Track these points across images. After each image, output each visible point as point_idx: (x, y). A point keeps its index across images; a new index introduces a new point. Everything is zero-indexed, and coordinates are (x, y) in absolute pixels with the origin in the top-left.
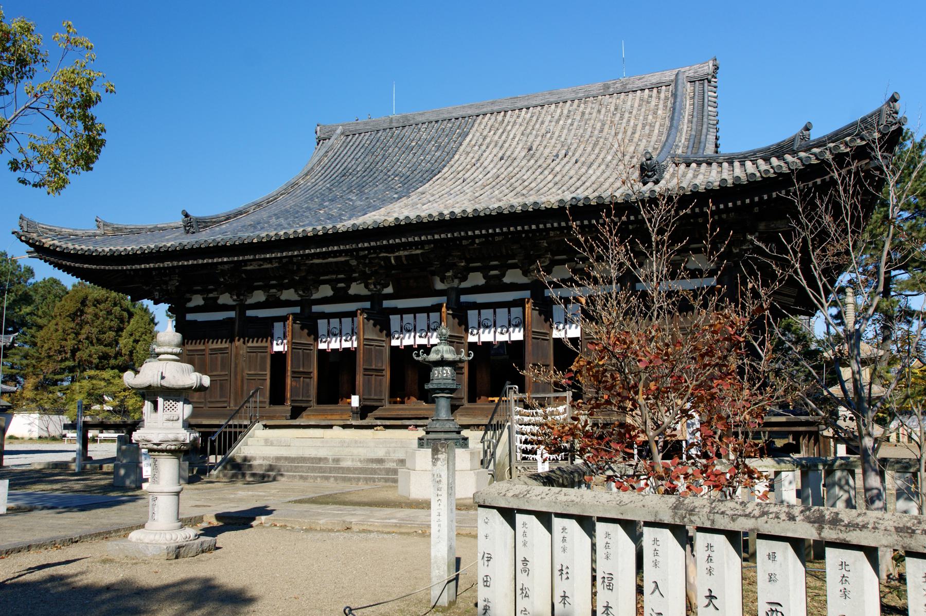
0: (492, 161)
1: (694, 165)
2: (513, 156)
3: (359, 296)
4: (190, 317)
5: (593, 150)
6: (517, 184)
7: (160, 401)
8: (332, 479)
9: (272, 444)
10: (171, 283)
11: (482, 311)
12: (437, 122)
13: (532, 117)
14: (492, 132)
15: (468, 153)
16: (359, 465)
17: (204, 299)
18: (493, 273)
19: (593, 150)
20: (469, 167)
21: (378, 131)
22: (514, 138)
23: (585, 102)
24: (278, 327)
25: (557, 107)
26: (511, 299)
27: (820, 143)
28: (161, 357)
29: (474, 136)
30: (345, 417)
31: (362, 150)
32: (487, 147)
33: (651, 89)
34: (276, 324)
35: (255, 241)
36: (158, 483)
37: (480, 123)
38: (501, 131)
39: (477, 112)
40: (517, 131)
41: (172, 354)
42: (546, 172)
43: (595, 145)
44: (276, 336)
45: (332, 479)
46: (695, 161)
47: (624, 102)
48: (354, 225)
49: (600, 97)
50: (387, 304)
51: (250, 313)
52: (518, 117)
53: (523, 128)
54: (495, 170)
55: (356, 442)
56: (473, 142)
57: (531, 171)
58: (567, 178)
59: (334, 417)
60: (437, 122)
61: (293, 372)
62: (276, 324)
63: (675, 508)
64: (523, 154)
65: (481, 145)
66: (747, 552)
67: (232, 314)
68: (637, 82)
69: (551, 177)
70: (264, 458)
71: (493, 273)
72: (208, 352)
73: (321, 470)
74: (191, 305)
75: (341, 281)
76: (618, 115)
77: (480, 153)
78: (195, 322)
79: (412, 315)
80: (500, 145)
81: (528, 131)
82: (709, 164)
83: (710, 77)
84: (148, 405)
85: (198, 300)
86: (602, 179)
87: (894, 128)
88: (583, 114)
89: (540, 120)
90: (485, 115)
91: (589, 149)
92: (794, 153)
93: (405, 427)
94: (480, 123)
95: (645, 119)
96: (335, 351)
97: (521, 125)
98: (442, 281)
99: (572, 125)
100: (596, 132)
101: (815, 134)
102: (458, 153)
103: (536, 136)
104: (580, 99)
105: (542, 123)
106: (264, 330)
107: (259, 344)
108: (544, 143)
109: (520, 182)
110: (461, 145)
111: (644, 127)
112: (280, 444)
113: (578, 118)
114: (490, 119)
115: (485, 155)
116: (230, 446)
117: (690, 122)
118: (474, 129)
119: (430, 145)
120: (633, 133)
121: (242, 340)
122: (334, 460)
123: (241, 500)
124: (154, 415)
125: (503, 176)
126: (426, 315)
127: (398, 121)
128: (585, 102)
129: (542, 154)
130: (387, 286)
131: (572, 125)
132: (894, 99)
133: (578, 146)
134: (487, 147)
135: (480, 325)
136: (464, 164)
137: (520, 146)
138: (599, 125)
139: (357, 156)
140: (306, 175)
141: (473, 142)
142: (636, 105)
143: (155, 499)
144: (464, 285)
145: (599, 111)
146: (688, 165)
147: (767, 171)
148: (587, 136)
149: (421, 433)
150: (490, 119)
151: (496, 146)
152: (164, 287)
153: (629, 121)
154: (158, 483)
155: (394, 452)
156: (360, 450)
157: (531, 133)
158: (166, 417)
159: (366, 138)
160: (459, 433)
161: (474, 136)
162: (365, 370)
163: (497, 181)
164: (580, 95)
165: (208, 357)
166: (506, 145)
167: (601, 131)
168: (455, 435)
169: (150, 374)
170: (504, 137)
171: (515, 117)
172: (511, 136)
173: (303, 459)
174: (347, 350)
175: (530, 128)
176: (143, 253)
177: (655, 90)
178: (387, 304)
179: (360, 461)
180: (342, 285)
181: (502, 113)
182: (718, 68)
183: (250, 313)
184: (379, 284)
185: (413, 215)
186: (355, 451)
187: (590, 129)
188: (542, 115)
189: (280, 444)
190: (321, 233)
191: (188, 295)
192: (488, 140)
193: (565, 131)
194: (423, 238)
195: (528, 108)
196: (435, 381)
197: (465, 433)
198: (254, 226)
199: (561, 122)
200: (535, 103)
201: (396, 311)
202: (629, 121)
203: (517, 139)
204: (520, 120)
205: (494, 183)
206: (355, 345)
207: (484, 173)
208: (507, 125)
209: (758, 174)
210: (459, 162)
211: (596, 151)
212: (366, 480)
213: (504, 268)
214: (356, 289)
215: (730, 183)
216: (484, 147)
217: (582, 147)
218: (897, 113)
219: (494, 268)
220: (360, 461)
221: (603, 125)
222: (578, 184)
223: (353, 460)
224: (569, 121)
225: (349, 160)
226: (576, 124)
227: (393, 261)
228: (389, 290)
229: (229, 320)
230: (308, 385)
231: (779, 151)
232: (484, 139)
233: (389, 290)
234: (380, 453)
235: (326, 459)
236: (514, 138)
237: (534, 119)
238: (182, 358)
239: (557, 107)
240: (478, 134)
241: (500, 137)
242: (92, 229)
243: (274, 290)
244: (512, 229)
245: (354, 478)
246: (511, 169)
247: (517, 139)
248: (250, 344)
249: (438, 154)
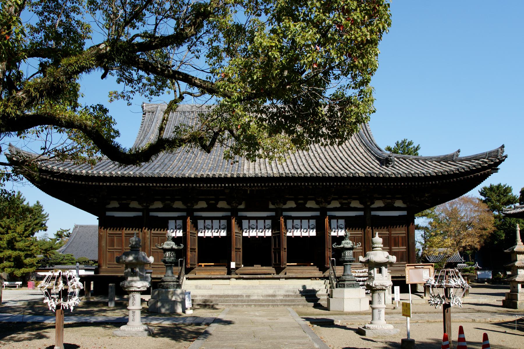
3: (179, 208)
4: (109, 214)
8: (253, 306)
9: (200, 288)
11: (295, 221)
16: (261, 298)
18: (300, 202)
24: (172, 223)
26: (176, 216)
30: (222, 273)
34: (170, 221)
44: (170, 228)
45: (253, 306)
55: (253, 286)
59: (215, 274)
61: (191, 249)
62: (170, 221)
70: (202, 296)
71: (300, 202)
72: (124, 235)
73: (242, 301)
74: (110, 206)
75: (212, 199)
78: (113, 217)
79: (255, 221)
96: (254, 237)
98: (273, 204)
101: (461, 155)
106: (163, 224)
112: (205, 288)
121: (140, 230)
122: (246, 296)
126: (307, 220)
130: (241, 204)
135: (249, 228)
147: (300, 174)
156: (259, 290)
162: (236, 248)
165: (124, 238)
173: (228, 296)
178: (241, 214)
179: (262, 296)
180: (213, 202)
183: (152, 214)
186: (256, 291)
189: (205, 288)
194: (165, 185)
209: (284, 174)
212: (273, 305)
214: (222, 204)
219: (301, 199)
220: (262, 296)
223: (258, 296)
228: (242, 206)
230: (195, 255)
231: (446, 159)
233: (242, 206)
234: (271, 292)
235: (241, 295)
243: (169, 202)
244: (176, 185)
245: (266, 305)
248: (153, 232)
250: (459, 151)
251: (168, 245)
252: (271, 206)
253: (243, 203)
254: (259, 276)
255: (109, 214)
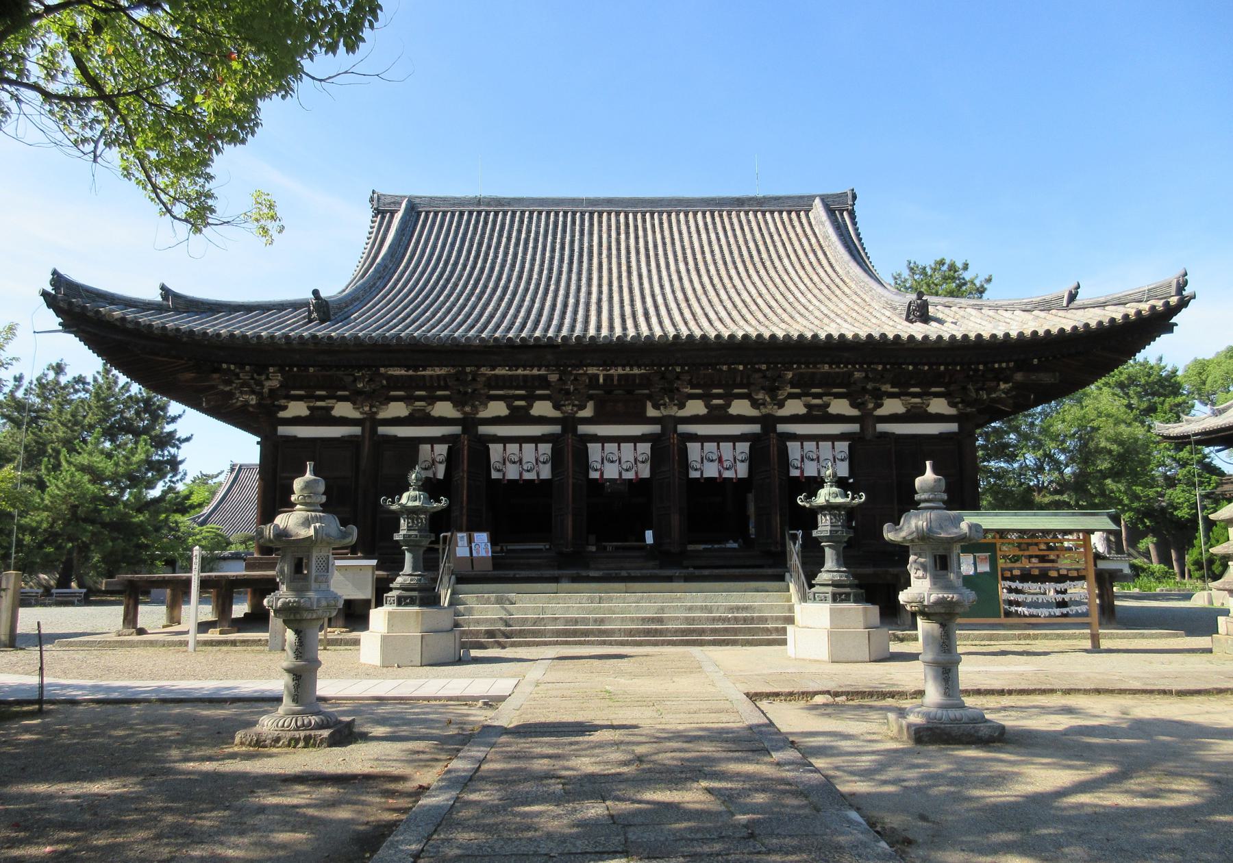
4: (283, 430)
11: (508, 446)
17: (309, 408)
50: (583, 429)
51: (382, 430)
66: (281, 611)
67: (356, 430)
78: (295, 439)
85: (298, 409)
98: (656, 407)
132: (17, 359)
144: (682, 413)
178: (583, 429)
183: (382, 430)
191: (283, 402)
201: (595, 438)
213: (729, 397)
219: (718, 396)
227: (601, 380)
228: (588, 412)
233: (588, 412)
242: (155, 296)
243: (423, 403)
252: (651, 412)
253: (590, 405)
255: (283, 430)
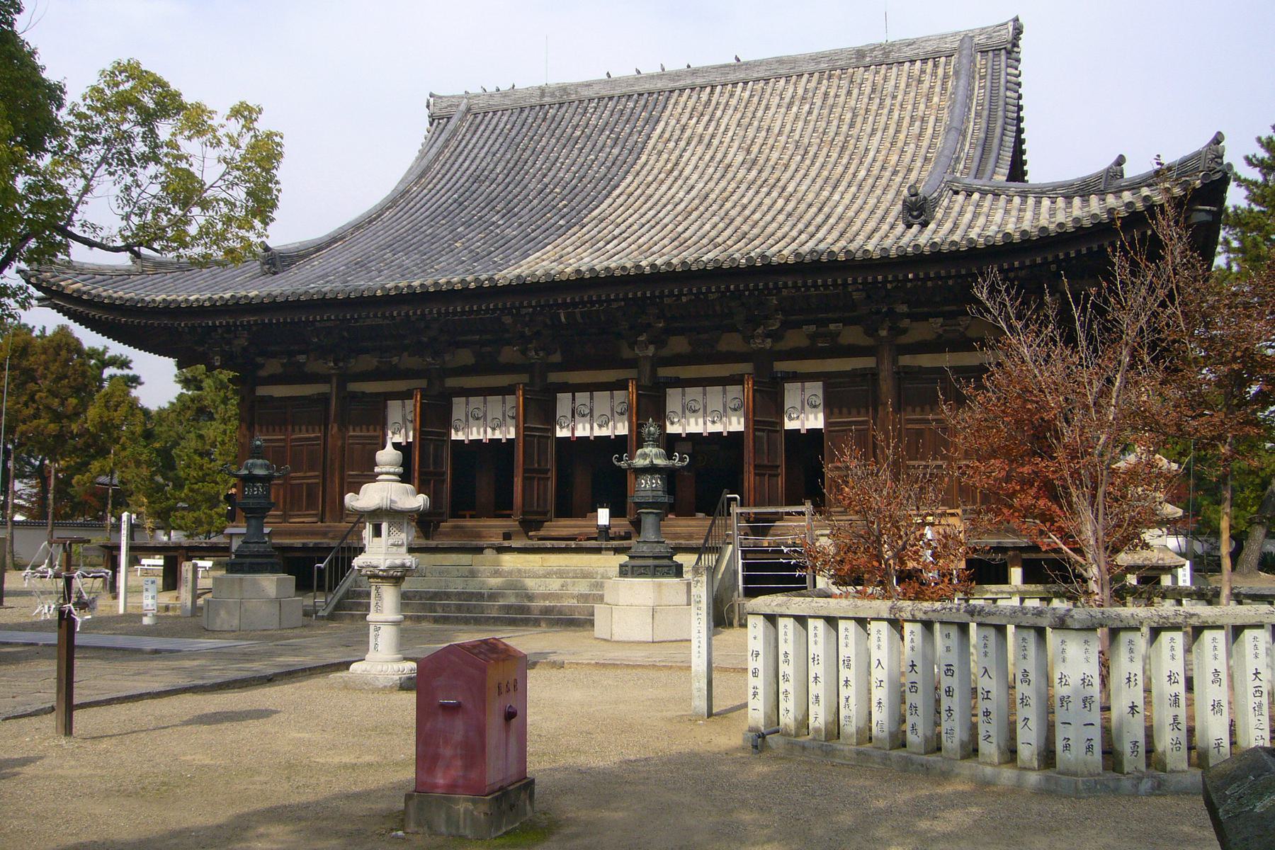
0: (696, 167)
1: (976, 196)
2: (727, 161)
4: (262, 391)
5: (840, 157)
6: (733, 213)
7: (384, 526)
10: (236, 342)
12: (611, 98)
13: (751, 96)
14: (694, 120)
15: (660, 153)
19: (840, 157)
20: (662, 176)
21: (522, 110)
22: (726, 130)
23: (830, 77)
25: (787, 82)
27: (1134, 186)
28: (380, 477)
29: (667, 124)
31: (501, 140)
32: (688, 144)
33: (924, 61)
35: (379, 293)
36: (382, 612)
37: (676, 103)
38: (706, 118)
39: (671, 85)
40: (729, 119)
41: (393, 474)
42: (775, 194)
43: (843, 148)
44: (390, 422)
46: (978, 190)
47: (885, 79)
48: (519, 277)
49: (851, 70)
50: (554, 377)
52: (731, 96)
53: (739, 115)
54: (701, 185)
56: (666, 135)
57: (754, 188)
58: (803, 206)
60: (611, 98)
63: (892, 608)
64: (740, 158)
65: (679, 139)
68: (906, 49)
69: (781, 202)
74: (263, 373)
76: (877, 101)
77: (677, 152)
80: (706, 141)
81: (747, 120)
82: (996, 195)
83: (1009, 46)
84: (368, 532)
85: (273, 367)
86: (851, 213)
87: (1218, 176)
88: (826, 94)
89: (764, 103)
90: (682, 90)
91: (835, 155)
92: (1102, 194)
93: (598, 550)
94: (676, 103)
95: (915, 108)
97: (736, 109)
99: (810, 113)
100: (845, 128)
101: (1131, 171)
102: (646, 152)
103: (759, 129)
104: (822, 72)
105: (767, 108)
107: (371, 433)
108: (771, 141)
109: (738, 208)
110: (649, 138)
111: (911, 124)
113: (818, 101)
114: (690, 97)
115: (687, 155)
116: (343, 575)
117: (978, 115)
118: (667, 113)
119: (604, 137)
120: (897, 132)
123: (210, 678)
124: (376, 539)
125: (713, 196)
127: (553, 95)
128: (830, 77)
129: (768, 160)
131: (810, 113)
133: (819, 149)
134: (688, 144)
136: (655, 172)
137: (736, 144)
138: (848, 116)
139: (494, 149)
140: (421, 176)
141: (666, 135)
142: (903, 86)
143: (377, 629)
145: (849, 93)
146: (969, 195)
148: (832, 134)
149: (624, 558)
150: (690, 97)
151: (700, 141)
152: (227, 348)
153: (891, 111)
154: (382, 612)
155: (574, 584)
157: (750, 124)
158: (391, 541)
159: (505, 118)
160: (671, 558)
161: (668, 122)
163: (706, 204)
164: (823, 66)
166: (715, 142)
167: (852, 126)
168: (666, 562)
169: (370, 497)
170: (711, 129)
171: (727, 95)
172: (722, 128)
174: (495, 442)
175: (749, 115)
176: (214, 305)
177: (930, 63)
180: (489, 349)
181: (708, 89)
182: (1021, 32)
184: (543, 349)
185: (600, 264)
187: (835, 123)
188: (767, 96)
190: (473, 285)
191: (259, 360)
192: (688, 133)
193: (800, 124)
195: (746, 83)
196: (642, 494)
197: (678, 558)
198: (361, 265)
199: (795, 109)
200: (755, 75)
202: (891, 111)
203: (730, 134)
204: (733, 102)
205: (702, 209)
206: (512, 435)
207: (685, 188)
208: (716, 109)
210: (648, 167)
211: (844, 161)
214: (509, 354)
215: (1017, 237)
216: (682, 144)
217: (825, 151)
218: (1221, 157)
221: (855, 116)
222: (819, 219)
224: (806, 107)
225: (482, 155)
226: (815, 112)
227: (563, 319)
228: (556, 358)
229: (324, 399)
232: (683, 130)
233: (556, 358)
236: (726, 130)
237: (755, 99)
238: (405, 478)
239: (787, 82)
240: (673, 122)
241: (706, 128)
246: (723, 184)
247: (730, 134)
249: (616, 151)
250: (1121, 161)
251: (645, 456)
254: (563, 544)
255: (262, 391)
